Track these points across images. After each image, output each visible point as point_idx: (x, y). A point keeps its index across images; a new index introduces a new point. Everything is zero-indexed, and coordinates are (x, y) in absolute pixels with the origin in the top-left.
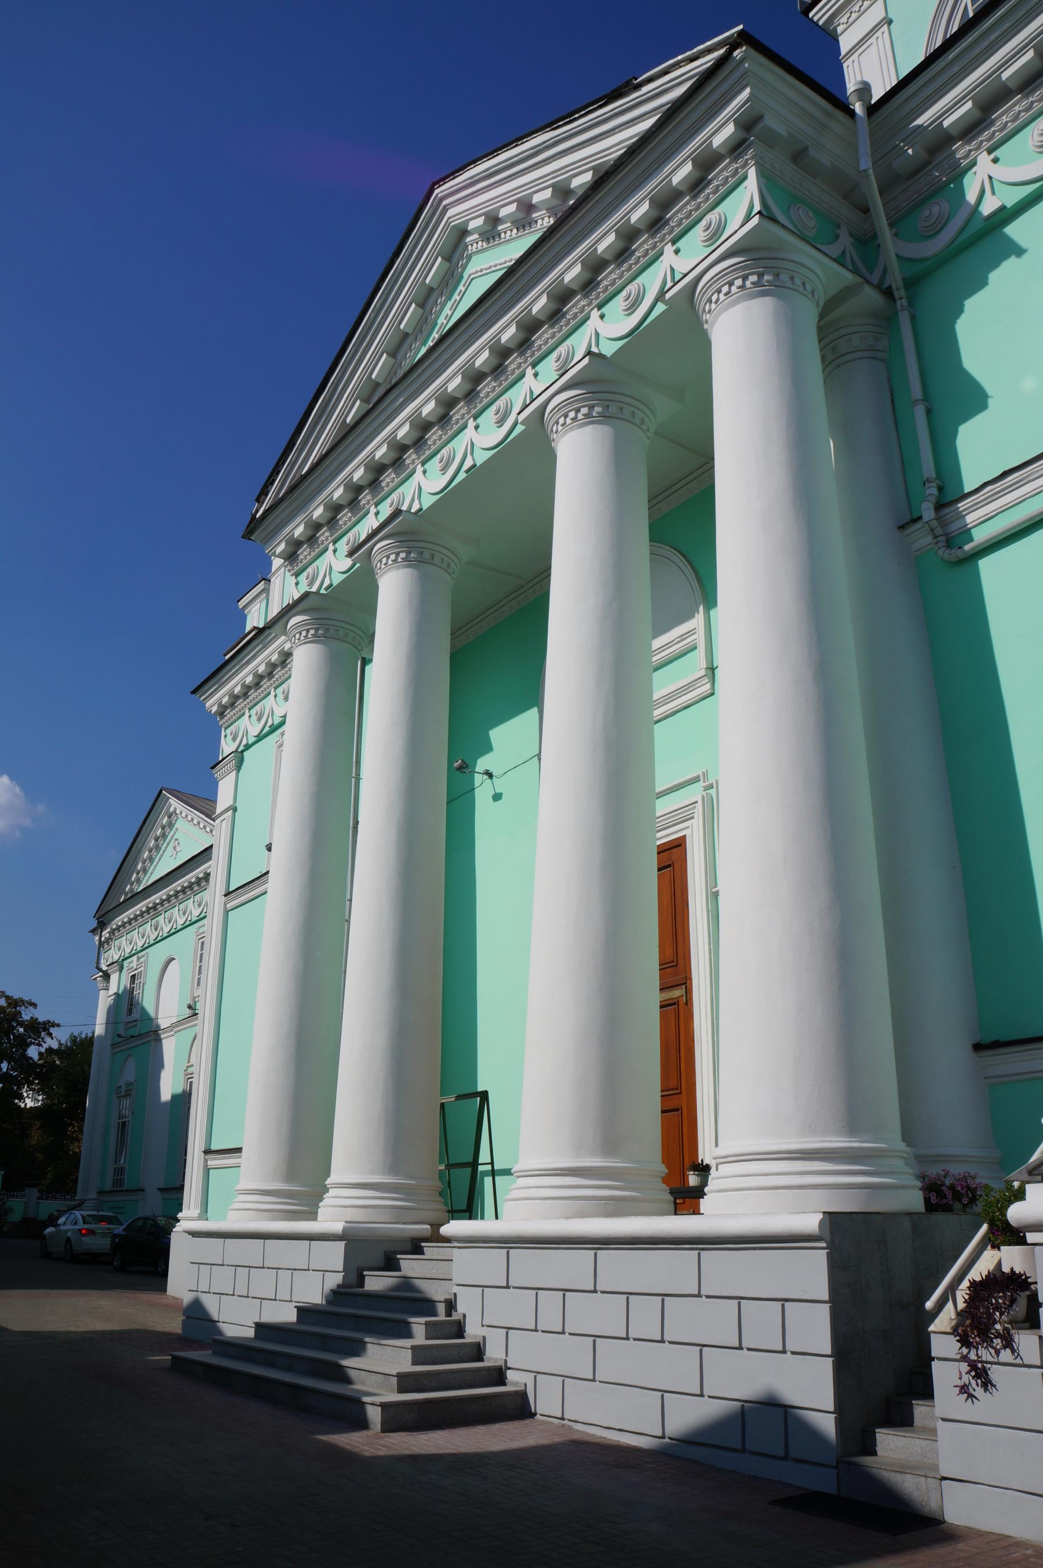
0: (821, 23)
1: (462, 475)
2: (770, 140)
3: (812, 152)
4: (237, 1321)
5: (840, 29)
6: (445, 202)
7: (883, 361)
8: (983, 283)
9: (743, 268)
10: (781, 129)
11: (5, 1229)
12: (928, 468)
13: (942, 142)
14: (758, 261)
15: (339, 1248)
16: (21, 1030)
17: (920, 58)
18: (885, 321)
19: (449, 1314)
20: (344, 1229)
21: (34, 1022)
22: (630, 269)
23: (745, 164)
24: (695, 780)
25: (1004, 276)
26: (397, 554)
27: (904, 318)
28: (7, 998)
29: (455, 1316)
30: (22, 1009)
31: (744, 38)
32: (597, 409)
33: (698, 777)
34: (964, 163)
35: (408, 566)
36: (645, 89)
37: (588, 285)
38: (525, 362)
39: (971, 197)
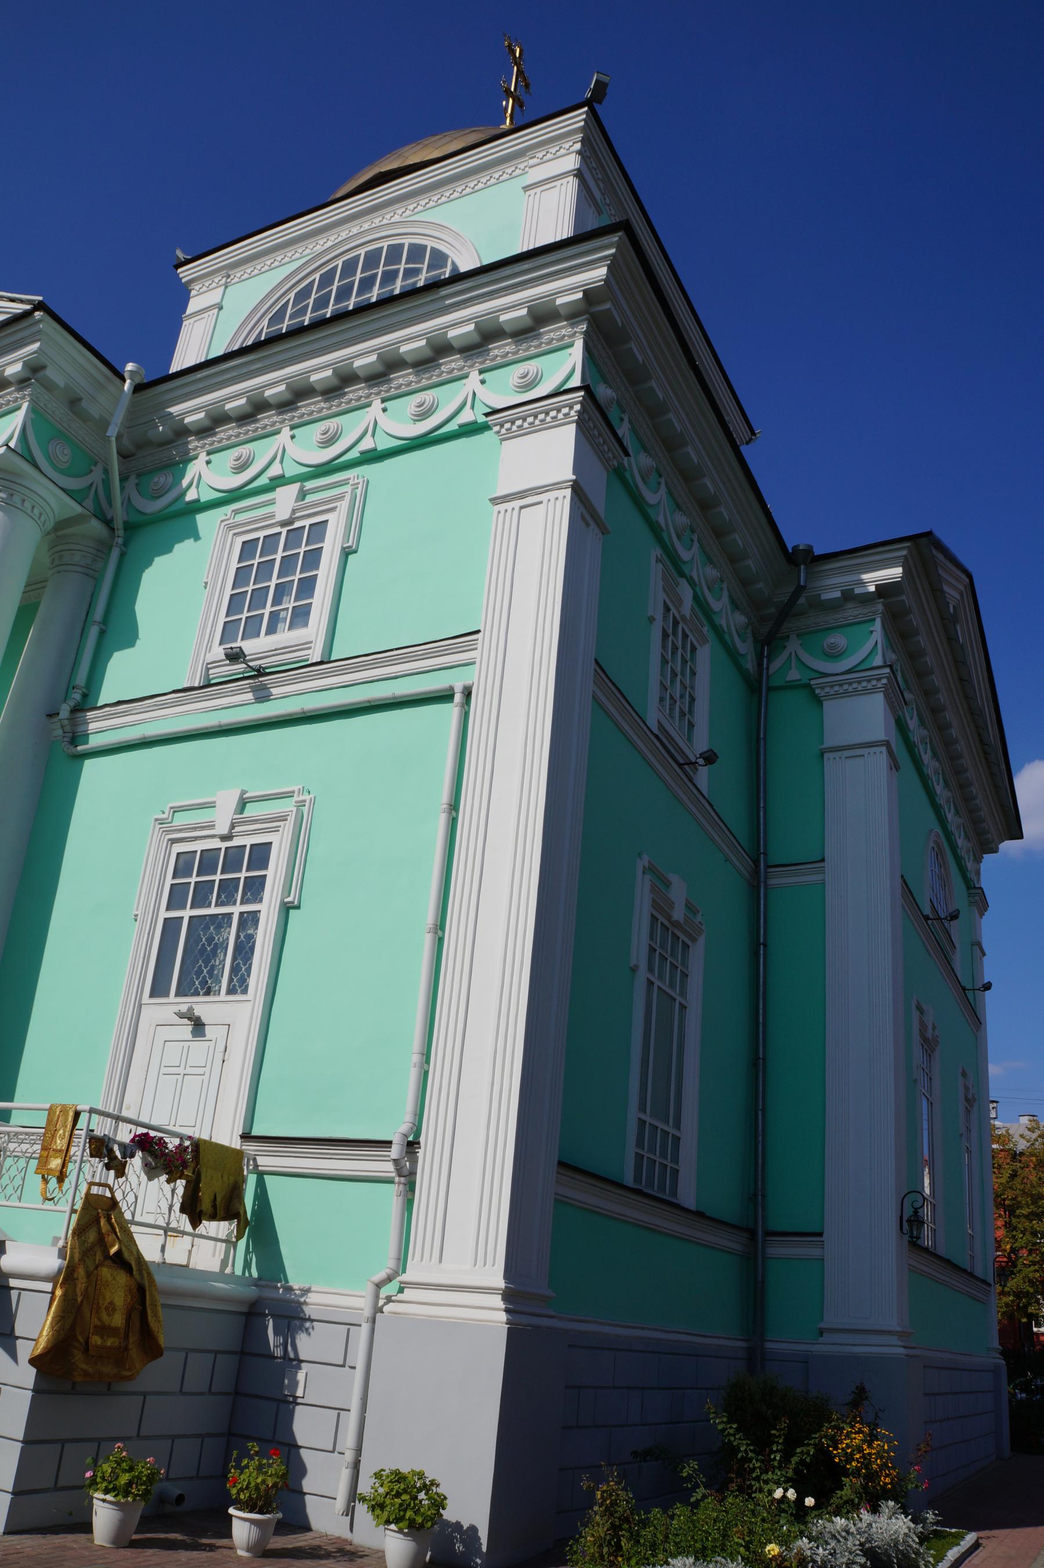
0: (183, 281)
2: (48, 386)
3: (84, 404)
4: (444, 1517)
5: (193, 293)
7: (94, 578)
8: (168, 550)
10: (60, 380)
12: (81, 678)
13: (182, 432)
17: (221, 353)
18: (103, 548)
23: (23, 398)
24: (289, 795)
25: (184, 549)
27: (115, 554)
31: (39, 306)
33: (293, 792)
34: (192, 453)
39: (185, 483)
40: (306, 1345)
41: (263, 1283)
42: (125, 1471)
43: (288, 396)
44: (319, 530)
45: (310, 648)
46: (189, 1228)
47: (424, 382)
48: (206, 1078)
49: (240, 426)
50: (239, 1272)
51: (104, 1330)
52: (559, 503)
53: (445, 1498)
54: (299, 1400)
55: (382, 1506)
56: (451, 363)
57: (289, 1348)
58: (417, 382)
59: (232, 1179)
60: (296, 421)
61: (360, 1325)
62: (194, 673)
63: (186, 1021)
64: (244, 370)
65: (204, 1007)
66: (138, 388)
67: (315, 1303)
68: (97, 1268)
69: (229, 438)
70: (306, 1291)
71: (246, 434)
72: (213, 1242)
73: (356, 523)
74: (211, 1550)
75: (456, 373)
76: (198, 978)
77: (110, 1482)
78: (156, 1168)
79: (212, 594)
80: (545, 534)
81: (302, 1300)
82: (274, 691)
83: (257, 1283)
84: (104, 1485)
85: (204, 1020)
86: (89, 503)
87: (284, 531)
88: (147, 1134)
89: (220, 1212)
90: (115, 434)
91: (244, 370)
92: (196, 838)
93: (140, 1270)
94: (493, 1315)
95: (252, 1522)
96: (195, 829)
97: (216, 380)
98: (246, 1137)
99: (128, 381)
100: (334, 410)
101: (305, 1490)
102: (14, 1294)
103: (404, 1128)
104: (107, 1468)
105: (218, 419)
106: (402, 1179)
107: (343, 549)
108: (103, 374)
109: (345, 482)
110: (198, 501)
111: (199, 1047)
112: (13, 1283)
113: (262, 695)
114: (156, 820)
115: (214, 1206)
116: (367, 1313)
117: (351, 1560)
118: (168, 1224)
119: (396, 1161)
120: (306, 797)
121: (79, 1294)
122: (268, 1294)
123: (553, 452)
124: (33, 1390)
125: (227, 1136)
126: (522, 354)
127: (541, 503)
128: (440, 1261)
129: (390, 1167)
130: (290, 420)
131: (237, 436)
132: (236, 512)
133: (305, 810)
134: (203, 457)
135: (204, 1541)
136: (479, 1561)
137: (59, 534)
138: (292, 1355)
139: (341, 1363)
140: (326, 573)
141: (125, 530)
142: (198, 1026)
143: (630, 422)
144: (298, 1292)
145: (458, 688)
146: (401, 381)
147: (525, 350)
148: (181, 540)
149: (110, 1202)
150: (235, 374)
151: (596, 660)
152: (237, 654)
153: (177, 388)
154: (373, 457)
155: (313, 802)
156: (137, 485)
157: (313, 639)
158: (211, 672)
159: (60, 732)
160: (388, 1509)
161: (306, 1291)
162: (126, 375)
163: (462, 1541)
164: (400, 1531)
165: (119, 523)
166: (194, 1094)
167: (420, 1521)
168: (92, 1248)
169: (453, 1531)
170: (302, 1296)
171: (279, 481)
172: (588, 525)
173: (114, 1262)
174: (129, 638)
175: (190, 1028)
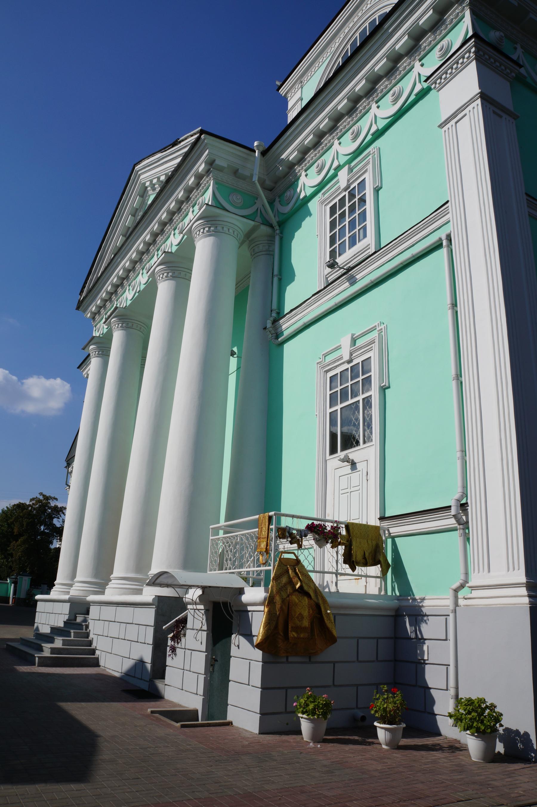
1: (137, 294)
2: (220, 169)
3: (240, 171)
6: (139, 173)
8: (299, 226)
9: (203, 225)
10: (224, 164)
11: (32, 603)
12: (275, 306)
13: (291, 166)
14: (211, 221)
15: (68, 605)
16: (50, 511)
18: (271, 239)
19: (86, 630)
20: (69, 598)
21: (56, 507)
22: (181, 216)
23: (210, 179)
26: (118, 324)
27: (277, 239)
28: (44, 496)
29: (88, 631)
30: (50, 501)
31: (202, 132)
32: (170, 274)
33: (376, 326)
35: (122, 330)
36: (182, 143)
37: (332, 129)
38: (302, 169)
39: (298, 190)
40: (428, 630)
41: (401, 598)
42: (311, 702)
43: (331, 124)
44: (362, 184)
45: (369, 248)
46: (349, 571)
47: (394, 82)
48: (360, 491)
49: (315, 150)
50: (389, 593)
51: (297, 629)
52: (475, 110)
53: (502, 715)
54: (427, 662)
55: (461, 720)
56: (404, 64)
57: (418, 632)
58: (390, 84)
59: (374, 543)
60: (339, 134)
61: (449, 615)
62: (320, 282)
63: (346, 463)
64: (307, 120)
65: (353, 454)
66: (264, 153)
67: (428, 606)
68: (288, 596)
69: (312, 159)
70: (423, 599)
71: (319, 152)
72: (374, 579)
73: (379, 173)
74: (369, 745)
75: (408, 68)
76: (350, 441)
77: (304, 708)
78: (320, 540)
79: (321, 239)
80: (472, 133)
81: (421, 604)
82: (357, 277)
83: (398, 598)
84: (302, 709)
85: (356, 461)
86: (258, 219)
87: (347, 193)
88: (313, 523)
89: (369, 561)
90: (257, 179)
91: (307, 120)
92: (337, 367)
93: (316, 596)
94: (521, 598)
95: (386, 729)
96: (335, 362)
97: (296, 132)
98: (382, 518)
99: (257, 151)
100: (355, 119)
101: (436, 712)
102: (250, 613)
103: (457, 496)
104: (302, 701)
105: (304, 152)
106: (461, 526)
107: (374, 189)
108: (240, 151)
109: (369, 154)
110: (306, 196)
111: (355, 476)
112: (249, 608)
113: (353, 281)
114: (318, 363)
115: (364, 558)
116: (452, 607)
117: (453, 752)
118: (337, 570)
119: (454, 516)
120: (382, 326)
121: (277, 610)
122: (404, 603)
123: (467, 82)
124: (263, 662)
125: (373, 521)
126: (438, 38)
127: (465, 115)
128: (489, 571)
129: (453, 521)
130: (336, 136)
131: (315, 155)
132: (324, 194)
133: (383, 333)
134: (304, 173)
135: (370, 740)
136: (533, 755)
137: (248, 238)
138: (420, 637)
139: (444, 638)
140: (369, 206)
141: (279, 226)
142: (353, 465)
143: (522, 47)
144: (419, 601)
145: (444, 237)
146: (382, 87)
147: (439, 35)
148: (304, 219)
149: (296, 561)
150: (303, 124)
151: (526, 194)
152: (332, 263)
153: (281, 144)
154: (379, 134)
155: (386, 328)
156: (280, 201)
157: (370, 242)
158: (329, 279)
159: (270, 336)
160: (464, 721)
161: (423, 599)
162: (255, 148)
163: (521, 742)
164: (473, 735)
165: (275, 224)
166: (352, 502)
167: (483, 728)
168: (285, 585)
169: (515, 736)
170: (421, 602)
171: (339, 168)
172: (501, 117)
173: (299, 592)
174: (291, 277)
175: (350, 467)
